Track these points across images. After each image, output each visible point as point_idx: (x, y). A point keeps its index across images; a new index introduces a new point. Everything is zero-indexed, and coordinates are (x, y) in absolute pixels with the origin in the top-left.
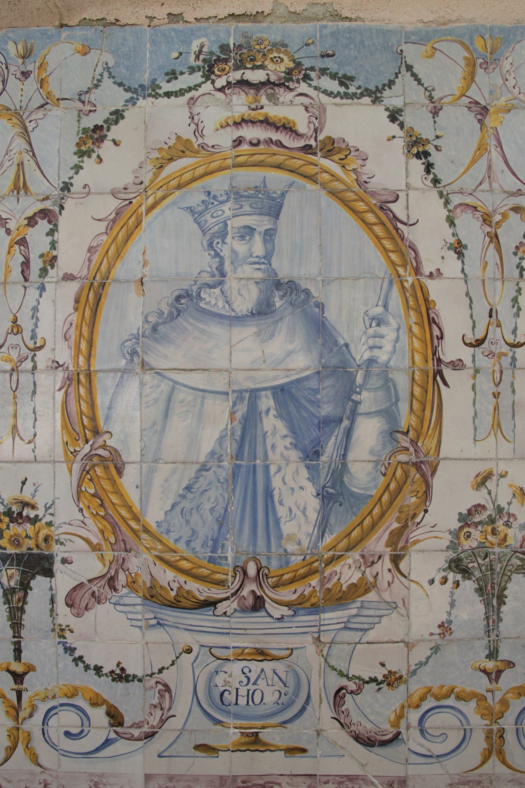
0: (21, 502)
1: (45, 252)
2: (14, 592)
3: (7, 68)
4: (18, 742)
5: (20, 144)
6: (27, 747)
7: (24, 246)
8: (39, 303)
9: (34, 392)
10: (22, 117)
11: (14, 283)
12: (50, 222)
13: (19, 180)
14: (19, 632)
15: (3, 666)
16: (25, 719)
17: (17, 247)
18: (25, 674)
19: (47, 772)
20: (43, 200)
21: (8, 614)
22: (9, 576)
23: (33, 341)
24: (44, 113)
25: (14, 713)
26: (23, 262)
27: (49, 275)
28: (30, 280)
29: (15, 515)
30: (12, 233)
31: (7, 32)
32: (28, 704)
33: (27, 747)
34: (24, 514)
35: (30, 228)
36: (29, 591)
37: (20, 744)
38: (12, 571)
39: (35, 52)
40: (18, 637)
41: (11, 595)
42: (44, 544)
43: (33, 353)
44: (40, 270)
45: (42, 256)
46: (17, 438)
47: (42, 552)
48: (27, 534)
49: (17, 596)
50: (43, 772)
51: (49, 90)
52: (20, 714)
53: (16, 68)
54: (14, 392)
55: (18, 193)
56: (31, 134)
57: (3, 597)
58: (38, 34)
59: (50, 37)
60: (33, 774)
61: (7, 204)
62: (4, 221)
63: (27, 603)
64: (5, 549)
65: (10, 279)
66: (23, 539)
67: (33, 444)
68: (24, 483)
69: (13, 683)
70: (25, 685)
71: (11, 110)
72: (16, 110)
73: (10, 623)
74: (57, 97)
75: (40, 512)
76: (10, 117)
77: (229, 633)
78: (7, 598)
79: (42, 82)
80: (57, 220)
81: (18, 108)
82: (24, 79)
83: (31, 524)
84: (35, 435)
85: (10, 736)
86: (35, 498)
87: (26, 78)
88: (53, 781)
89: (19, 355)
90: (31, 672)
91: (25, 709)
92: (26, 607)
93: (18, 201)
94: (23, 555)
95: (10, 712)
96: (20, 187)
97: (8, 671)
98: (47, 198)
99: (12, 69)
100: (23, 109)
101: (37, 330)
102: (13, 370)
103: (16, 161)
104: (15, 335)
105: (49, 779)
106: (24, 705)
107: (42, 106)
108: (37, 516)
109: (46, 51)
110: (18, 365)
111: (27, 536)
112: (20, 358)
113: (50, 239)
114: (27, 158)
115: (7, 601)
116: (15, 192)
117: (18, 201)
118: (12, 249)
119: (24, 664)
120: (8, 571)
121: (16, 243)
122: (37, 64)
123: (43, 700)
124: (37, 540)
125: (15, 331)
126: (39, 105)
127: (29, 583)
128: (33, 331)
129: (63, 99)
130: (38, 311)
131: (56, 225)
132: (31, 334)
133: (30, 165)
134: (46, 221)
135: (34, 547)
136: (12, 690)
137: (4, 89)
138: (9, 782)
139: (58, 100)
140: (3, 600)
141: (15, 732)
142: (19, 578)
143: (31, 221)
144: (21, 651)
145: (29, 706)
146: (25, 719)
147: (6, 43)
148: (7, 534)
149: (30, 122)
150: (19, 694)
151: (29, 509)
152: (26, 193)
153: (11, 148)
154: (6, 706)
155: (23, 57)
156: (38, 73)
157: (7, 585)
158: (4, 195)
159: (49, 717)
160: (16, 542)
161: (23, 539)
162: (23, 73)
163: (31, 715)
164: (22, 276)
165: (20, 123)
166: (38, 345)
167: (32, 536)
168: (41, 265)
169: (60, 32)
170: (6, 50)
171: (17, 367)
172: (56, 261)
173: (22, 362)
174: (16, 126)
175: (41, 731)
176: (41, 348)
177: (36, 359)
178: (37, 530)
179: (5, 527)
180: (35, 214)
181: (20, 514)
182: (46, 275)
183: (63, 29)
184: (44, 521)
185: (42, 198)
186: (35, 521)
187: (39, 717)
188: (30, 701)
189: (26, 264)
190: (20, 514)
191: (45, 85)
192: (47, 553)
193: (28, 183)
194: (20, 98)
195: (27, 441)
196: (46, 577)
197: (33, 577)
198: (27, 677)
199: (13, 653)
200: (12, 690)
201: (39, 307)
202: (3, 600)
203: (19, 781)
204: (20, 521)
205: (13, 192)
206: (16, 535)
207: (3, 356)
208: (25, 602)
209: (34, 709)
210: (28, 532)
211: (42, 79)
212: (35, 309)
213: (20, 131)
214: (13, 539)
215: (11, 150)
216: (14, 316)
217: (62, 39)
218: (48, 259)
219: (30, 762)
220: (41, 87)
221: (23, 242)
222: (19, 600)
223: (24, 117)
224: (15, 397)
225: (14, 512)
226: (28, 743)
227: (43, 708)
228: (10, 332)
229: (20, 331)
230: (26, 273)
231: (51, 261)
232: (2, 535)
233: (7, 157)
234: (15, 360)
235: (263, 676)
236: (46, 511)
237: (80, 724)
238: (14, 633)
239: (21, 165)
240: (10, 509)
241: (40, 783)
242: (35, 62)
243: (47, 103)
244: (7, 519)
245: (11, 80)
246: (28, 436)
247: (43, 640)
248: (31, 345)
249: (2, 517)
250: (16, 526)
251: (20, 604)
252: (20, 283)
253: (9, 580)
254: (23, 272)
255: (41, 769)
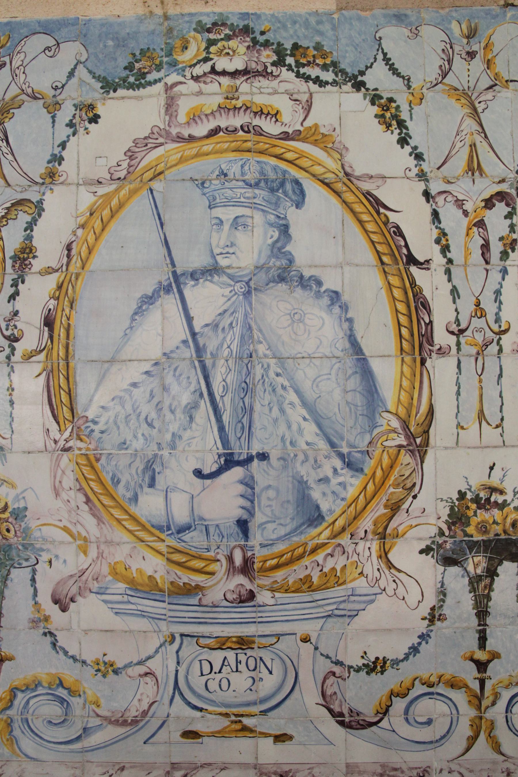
0: (489, 488)
1: (504, 235)
2: (481, 580)
3: (451, 47)
4: (480, 731)
5: (470, 125)
6: (489, 735)
7: (482, 228)
8: (501, 287)
9: (500, 376)
10: (470, 98)
11: (474, 265)
12: (508, 205)
13: (472, 162)
14: (484, 620)
15: (467, 655)
16: (487, 707)
17: (475, 229)
18: (489, 661)
19: (509, 760)
20: (500, 182)
21: (473, 602)
22: (476, 563)
23: (497, 325)
24: (494, 94)
25: (477, 702)
26: (483, 245)
27: (510, 258)
28: (491, 263)
29: (483, 502)
30: (469, 214)
31: (451, 11)
32: (491, 692)
33: (489, 735)
34: (492, 499)
35: (488, 211)
36: (495, 577)
37: (482, 733)
38: (479, 558)
39: (479, 32)
40: (483, 625)
41: (477, 582)
42: (511, 529)
43: (498, 337)
44: (501, 253)
45: (501, 239)
46: (484, 423)
47: (510, 537)
48: (494, 520)
49: (483, 583)
50: (505, 761)
51: (497, 71)
52: (483, 703)
53: (461, 48)
54: (480, 376)
55: (473, 174)
56: (481, 115)
57: (469, 586)
58: (482, 13)
59: (495, 17)
60: (494, 763)
61: (462, 186)
62: (460, 203)
63: (493, 591)
64: (472, 536)
65: (470, 261)
66: (490, 525)
67: (500, 428)
68: (491, 468)
69: (477, 672)
70: (488, 673)
71: (459, 90)
72: (464, 90)
73: (475, 611)
74: (506, 79)
75: (509, 497)
76: (458, 97)
77: (255, 622)
78: (473, 586)
79: (489, 63)
80: (514, 203)
81: (466, 88)
82: (469, 59)
83: (498, 510)
84: (502, 419)
85: (472, 725)
86: (503, 483)
87: (472, 59)
88: (516, 769)
89: (484, 339)
90: (496, 660)
91: (488, 697)
92: (492, 594)
93: (474, 183)
94: (490, 541)
95: (473, 701)
96: (474, 169)
97: (472, 660)
98: (503, 181)
99: (457, 48)
100: (472, 89)
101: (501, 313)
102: (478, 353)
103: (468, 142)
104: (479, 318)
105: (512, 767)
106: (486, 694)
107: (491, 87)
108: (505, 501)
109: (490, 31)
110: (483, 349)
111: (495, 522)
112: (485, 342)
113: (508, 222)
114: (478, 139)
115: (473, 590)
116: (470, 173)
117: (474, 183)
118: (470, 231)
119: (489, 652)
120: (474, 558)
121: (474, 225)
122: (483, 45)
123: (507, 687)
124: (504, 525)
125: (479, 314)
126: (487, 86)
127: (496, 569)
128: (497, 314)
129: (512, 81)
130: (501, 294)
131: (514, 208)
132: (495, 317)
133: (482, 147)
134: (503, 204)
135: (502, 532)
136: (475, 679)
137: (450, 69)
138: (471, 771)
139: (507, 81)
140: (469, 588)
141: (477, 721)
142: (486, 565)
143: (489, 204)
144: (486, 639)
145: (492, 694)
146: (487, 707)
147: (450, 23)
148: (474, 521)
149: (480, 103)
150: (482, 683)
151: (498, 495)
152: (481, 175)
153: (461, 129)
154: (468, 696)
155: (468, 37)
156: (484, 53)
157: (473, 573)
158: (459, 176)
159: (512, 704)
160: (483, 528)
161: (490, 525)
162: (468, 53)
163: (494, 703)
164: (482, 259)
165: (469, 104)
166: (503, 328)
167: (499, 522)
168: (502, 249)
169: (505, 11)
170: (450, 29)
171: (483, 351)
172: (516, 244)
173: (487, 346)
174: (465, 106)
175: (505, 719)
176: (505, 331)
177: (501, 342)
178: (505, 515)
179: (473, 514)
180: (492, 196)
181: (488, 500)
182: (508, 258)
183: (507, 9)
184: (512, 506)
185: (497, 180)
186: (504, 505)
187: (502, 704)
188: (494, 689)
189: (486, 247)
190: (488, 500)
191: (492, 66)
192: (514, 538)
193: (483, 165)
194: (468, 79)
195: (494, 426)
196: (513, 562)
197: (500, 563)
198: (491, 665)
199: (478, 642)
200: (475, 679)
201: (502, 290)
202: (469, 588)
203: (481, 770)
204: (488, 507)
205: (467, 173)
206: (483, 521)
207: (467, 340)
208: (491, 589)
209: (497, 696)
210: (495, 518)
211: (489, 60)
212: (498, 293)
213: (469, 111)
214: (480, 526)
215: (462, 131)
216: (477, 299)
217: (507, 18)
218: (508, 242)
219: (492, 751)
220: (488, 68)
221: (481, 224)
222: (485, 587)
223: (473, 98)
224: (480, 381)
225: (482, 498)
226: (491, 732)
227: (506, 695)
228: (473, 315)
229: (484, 315)
230: (487, 256)
231: (511, 244)
232: (469, 522)
233: (458, 137)
234: (480, 343)
235: (226, 663)
236: (515, 496)
237: (450, 713)
238: (479, 621)
239: (473, 146)
240: (478, 495)
241: (503, 772)
242: (480, 42)
243: (496, 85)
244: (474, 506)
245: (457, 59)
246: (496, 421)
247: (508, 627)
248: (496, 328)
249: (470, 504)
250: (484, 513)
251: (486, 592)
252: (481, 265)
253: (475, 568)
254: (483, 254)
255: (502, 758)
